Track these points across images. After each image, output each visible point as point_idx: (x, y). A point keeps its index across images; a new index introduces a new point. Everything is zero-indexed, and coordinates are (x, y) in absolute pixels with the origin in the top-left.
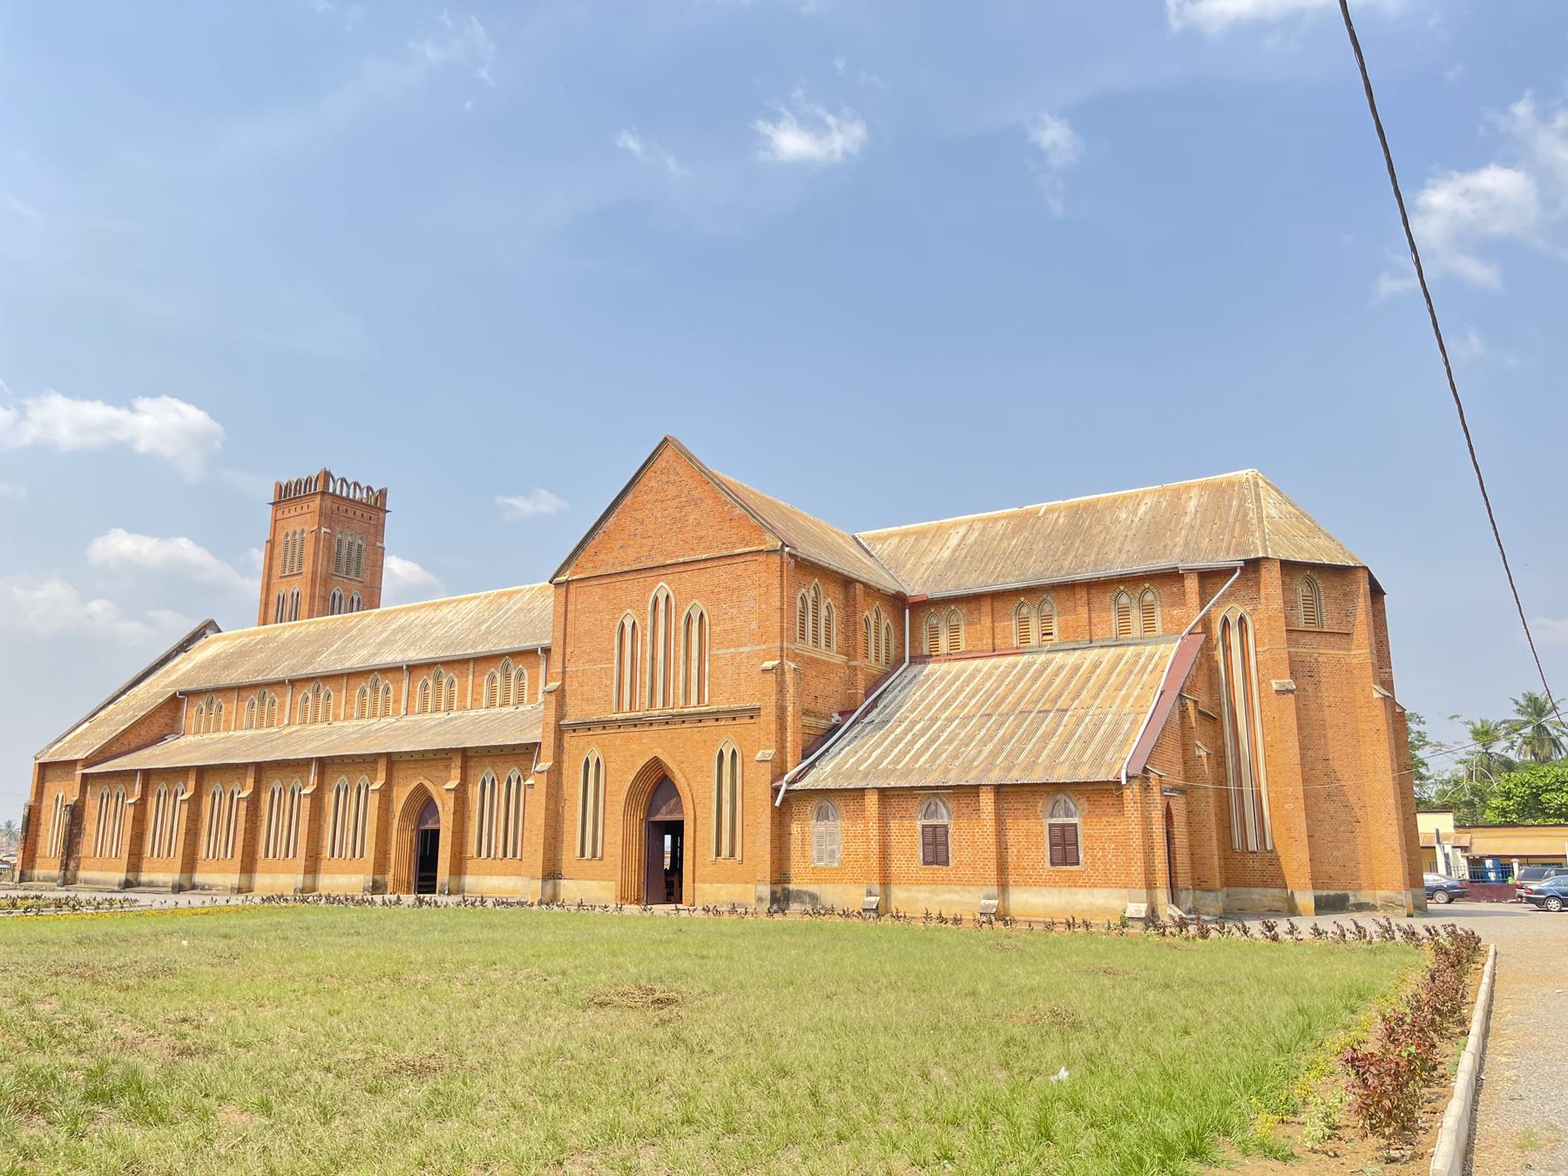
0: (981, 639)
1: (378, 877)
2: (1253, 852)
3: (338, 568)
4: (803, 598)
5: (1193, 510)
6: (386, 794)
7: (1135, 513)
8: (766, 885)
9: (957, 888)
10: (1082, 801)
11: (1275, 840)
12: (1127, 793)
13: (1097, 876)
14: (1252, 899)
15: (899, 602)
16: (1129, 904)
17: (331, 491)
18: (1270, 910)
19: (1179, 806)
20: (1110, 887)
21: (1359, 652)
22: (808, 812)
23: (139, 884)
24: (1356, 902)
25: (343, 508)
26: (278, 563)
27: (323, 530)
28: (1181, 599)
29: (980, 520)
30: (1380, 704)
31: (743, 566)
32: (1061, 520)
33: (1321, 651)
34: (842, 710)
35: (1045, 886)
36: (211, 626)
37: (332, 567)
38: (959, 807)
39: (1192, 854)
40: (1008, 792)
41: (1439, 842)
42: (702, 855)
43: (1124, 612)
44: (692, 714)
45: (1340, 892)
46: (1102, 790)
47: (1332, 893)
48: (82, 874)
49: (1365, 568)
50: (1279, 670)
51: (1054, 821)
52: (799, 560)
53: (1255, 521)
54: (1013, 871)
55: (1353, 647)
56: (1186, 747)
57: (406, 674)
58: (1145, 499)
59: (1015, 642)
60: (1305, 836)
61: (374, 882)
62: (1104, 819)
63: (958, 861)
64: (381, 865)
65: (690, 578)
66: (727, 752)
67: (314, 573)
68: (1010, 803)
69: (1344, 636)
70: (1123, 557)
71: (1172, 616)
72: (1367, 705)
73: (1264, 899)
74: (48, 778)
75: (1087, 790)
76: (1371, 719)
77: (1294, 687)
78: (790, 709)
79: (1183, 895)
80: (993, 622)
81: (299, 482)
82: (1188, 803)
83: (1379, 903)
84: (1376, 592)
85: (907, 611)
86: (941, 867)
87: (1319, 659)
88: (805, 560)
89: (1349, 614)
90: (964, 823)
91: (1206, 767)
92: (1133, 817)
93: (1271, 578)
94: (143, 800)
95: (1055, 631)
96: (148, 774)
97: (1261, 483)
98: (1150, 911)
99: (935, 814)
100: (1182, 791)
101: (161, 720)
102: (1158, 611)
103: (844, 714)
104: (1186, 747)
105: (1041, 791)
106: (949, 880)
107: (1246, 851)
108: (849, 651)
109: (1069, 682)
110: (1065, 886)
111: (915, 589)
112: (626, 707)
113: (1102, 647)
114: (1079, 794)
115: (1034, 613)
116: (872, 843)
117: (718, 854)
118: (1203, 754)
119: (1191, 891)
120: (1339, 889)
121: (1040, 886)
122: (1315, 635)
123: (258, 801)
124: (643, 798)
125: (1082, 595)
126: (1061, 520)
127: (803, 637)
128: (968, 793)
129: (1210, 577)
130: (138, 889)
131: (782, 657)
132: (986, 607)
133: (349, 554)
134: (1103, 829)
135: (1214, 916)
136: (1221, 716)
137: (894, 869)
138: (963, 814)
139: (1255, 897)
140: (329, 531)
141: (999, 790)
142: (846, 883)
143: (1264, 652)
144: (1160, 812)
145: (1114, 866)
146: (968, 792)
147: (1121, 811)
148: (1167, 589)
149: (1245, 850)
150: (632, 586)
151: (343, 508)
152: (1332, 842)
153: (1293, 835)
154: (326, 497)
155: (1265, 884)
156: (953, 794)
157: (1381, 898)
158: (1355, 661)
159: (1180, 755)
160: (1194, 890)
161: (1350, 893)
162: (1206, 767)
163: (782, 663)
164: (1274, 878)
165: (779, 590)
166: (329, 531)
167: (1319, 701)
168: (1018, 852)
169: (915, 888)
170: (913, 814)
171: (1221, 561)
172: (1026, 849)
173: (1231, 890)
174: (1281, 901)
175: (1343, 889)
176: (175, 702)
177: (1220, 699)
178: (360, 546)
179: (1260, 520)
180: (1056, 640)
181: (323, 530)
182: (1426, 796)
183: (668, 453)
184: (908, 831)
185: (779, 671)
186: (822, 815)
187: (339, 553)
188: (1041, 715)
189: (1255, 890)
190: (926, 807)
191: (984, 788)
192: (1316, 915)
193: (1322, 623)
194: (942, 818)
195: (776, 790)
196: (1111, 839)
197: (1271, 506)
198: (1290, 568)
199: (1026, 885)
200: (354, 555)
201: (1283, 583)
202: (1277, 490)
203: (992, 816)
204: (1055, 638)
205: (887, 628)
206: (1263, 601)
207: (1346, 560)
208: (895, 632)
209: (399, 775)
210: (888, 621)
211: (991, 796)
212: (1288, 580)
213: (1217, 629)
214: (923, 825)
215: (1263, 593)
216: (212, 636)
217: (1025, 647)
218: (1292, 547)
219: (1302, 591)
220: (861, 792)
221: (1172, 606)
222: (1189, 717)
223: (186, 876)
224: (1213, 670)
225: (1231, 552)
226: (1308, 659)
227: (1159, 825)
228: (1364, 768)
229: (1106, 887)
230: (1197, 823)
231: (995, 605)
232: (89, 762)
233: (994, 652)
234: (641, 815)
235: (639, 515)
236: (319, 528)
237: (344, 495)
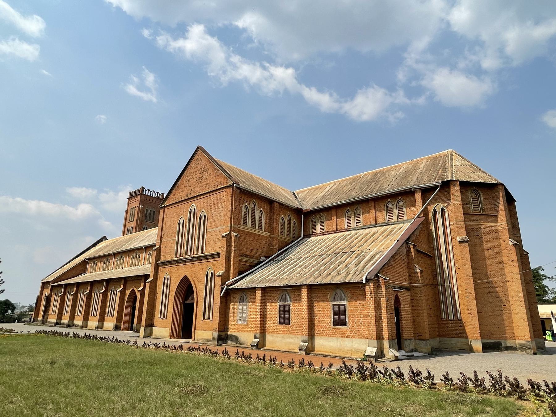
0: (332, 227)
1: (118, 324)
2: (451, 320)
3: (146, 219)
4: (283, 219)
5: (423, 167)
6: (123, 292)
7: (398, 171)
8: (216, 332)
9: (293, 336)
10: (348, 292)
11: (462, 314)
12: (367, 288)
13: (355, 332)
14: (452, 343)
15: (298, 212)
16: (368, 348)
17: (144, 193)
18: (460, 349)
19: (405, 297)
20: (361, 338)
21: (502, 223)
22: (237, 298)
23: (61, 324)
24: (506, 346)
25: (148, 199)
26: (128, 217)
27: (141, 206)
28: (414, 204)
29: (338, 181)
30: (513, 248)
31: (220, 194)
32: (369, 178)
33: (482, 224)
34: (267, 255)
35: (331, 336)
36: (105, 238)
37: (144, 219)
38: (295, 296)
39: (414, 321)
40: (315, 289)
41: (553, 316)
42: (199, 318)
43: (390, 211)
44: (204, 256)
45: (496, 341)
46: (357, 287)
47: (492, 341)
48: (49, 320)
49: (502, 185)
50: (460, 232)
51: (335, 303)
52: (242, 190)
53: (449, 167)
54: (317, 328)
55: (498, 221)
56: (410, 267)
57: (145, 250)
58: (404, 165)
59: (345, 227)
60: (476, 312)
61: (116, 325)
62: (358, 302)
63: (294, 323)
64: (119, 319)
65: (202, 200)
66: (210, 273)
67: (137, 220)
68: (316, 294)
69: (494, 217)
70: (390, 187)
71: (411, 211)
72: (507, 248)
73: (457, 343)
74: (45, 287)
75: (350, 287)
76: (509, 255)
77: (468, 239)
78: (233, 253)
79: (407, 343)
80: (336, 219)
81: (133, 192)
82: (411, 295)
83: (518, 346)
84: (510, 200)
85: (303, 216)
86: (286, 325)
87: (482, 227)
88: (246, 190)
89: (496, 206)
90: (296, 304)
91: (420, 277)
92: (370, 300)
93: (455, 192)
94: (64, 295)
95: (361, 221)
96: (66, 285)
97: (453, 154)
98: (380, 352)
99: (285, 300)
100: (407, 289)
101: (80, 268)
102: (405, 209)
103: (267, 257)
104: (410, 267)
105: (329, 288)
106: (289, 332)
107: (448, 320)
108: (271, 230)
109: (361, 240)
110: (340, 337)
111: (307, 206)
112: (178, 255)
113: (380, 226)
114: (346, 289)
115: (353, 214)
116: (258, 313)
117: (204, 317)
118: (418, 270)
119: (413, 340)
120: (496, 339)
121: (329, 336)
122: (479, 216)
123: (107, 295)
124: (183, 293)
125: (372, 204)
126: (369, 178)
127: (245, 222)
128: (298, 289)
129: (426, 192)
130: (61, 325)
131: (230, 231)
132: (334, 212)
133: (150, 214)
134: (358, 307)
135: (425, 353)
136: (434, 255)
137: (268, 326)
138: (296, 299)
139: (453, 342)
140: (143, 206)
141: (310, 287)
142: (249, 332)
143: (453, 224)
144: (385, 298)
145: (363, 327)
146: (297, 288)
147: (364, 299)
148: (408, 199)
149: (448, 319)
150: (184, 206)
151: (148, 199)
152: (491, 315)
153: (470, 312)
154: (142, 195)
155: (458, 336)
156: (293, 290)
157: (519, 344)
158: (499, 228)
159: (406, 271)
160: (415, 339)
161: (502, 341)
162: (420, 277)
163: (230, 233)
164: (462, 334)
165: (231, 202)
166: (143, 206)
167: (482, 247)
168: (319, 318)
169: (275, 335)
170: (276, 300)
171: (432, 183)
172: (323, 317)
173: (442, 339)
174: (466, 345)
175: (498, 339)
176: (85, 262)
177: (433, 247)
178: (154, 212)
179: (452, 166)
180: (362, 225)
181: (141, 206)
182: (548, 298)
183: (199, 152)
184: (273, 309)
185: (228, 237)
186: (242, 301)
187: (146, 214)
188: (343, 254)
189: (453, 339)
190: (281, 296)
191: (304, 286)
192: (483, 352)
193: (482, 211)
194: (288, 301)
195: (222, 289)
196: (361, 313)
197: (457, 162)
198: (465, 185)
199: (322, 336)
200: (152, 214)
201: (461, 192)
202: (461, 156)
203: (306, 300)
204: (361, 224)
205: (294, 223)
206: (452, 200)
207: (493, 181)
208: (298, 225)
209: (128, 285)
210: (295, 220)
211: (306, 290)
212: (464, 191)
213: (431, 215)
214: (280, 305)
215: (451, 197)
216: (104, 241)
217: (350, 229)
218: (466, 176)
219: (472, 196)
220: (254, 289)
221: (411, 206)
222: (411, 253)
223: (71, 321)
224: (430, 233)
225: (436, 180)
226: (476, 227)
227: (384, 305)
228: (507, 279)
229: (359, 338)
230: (416, 305)
231: (337, 211)
232: (54, 281)
233: (337, 231)
234: (181, 300)
235: (188, 178)
236: (140, 206)
237: (149, 195)
